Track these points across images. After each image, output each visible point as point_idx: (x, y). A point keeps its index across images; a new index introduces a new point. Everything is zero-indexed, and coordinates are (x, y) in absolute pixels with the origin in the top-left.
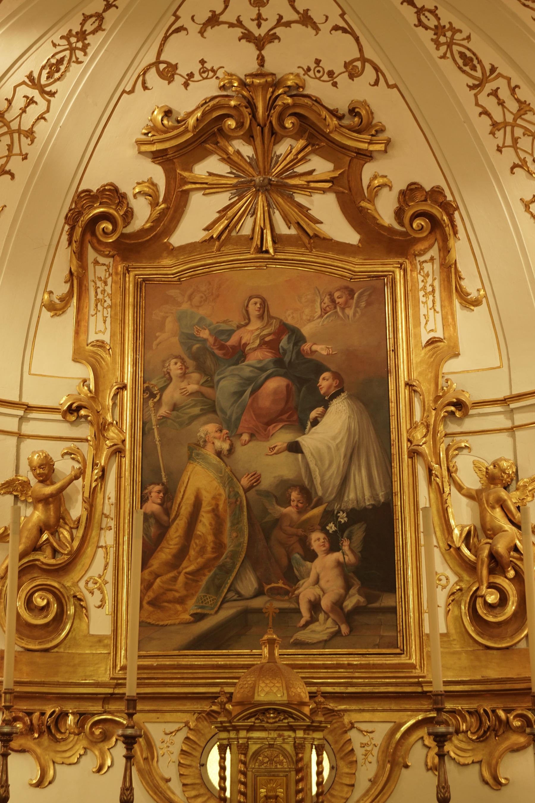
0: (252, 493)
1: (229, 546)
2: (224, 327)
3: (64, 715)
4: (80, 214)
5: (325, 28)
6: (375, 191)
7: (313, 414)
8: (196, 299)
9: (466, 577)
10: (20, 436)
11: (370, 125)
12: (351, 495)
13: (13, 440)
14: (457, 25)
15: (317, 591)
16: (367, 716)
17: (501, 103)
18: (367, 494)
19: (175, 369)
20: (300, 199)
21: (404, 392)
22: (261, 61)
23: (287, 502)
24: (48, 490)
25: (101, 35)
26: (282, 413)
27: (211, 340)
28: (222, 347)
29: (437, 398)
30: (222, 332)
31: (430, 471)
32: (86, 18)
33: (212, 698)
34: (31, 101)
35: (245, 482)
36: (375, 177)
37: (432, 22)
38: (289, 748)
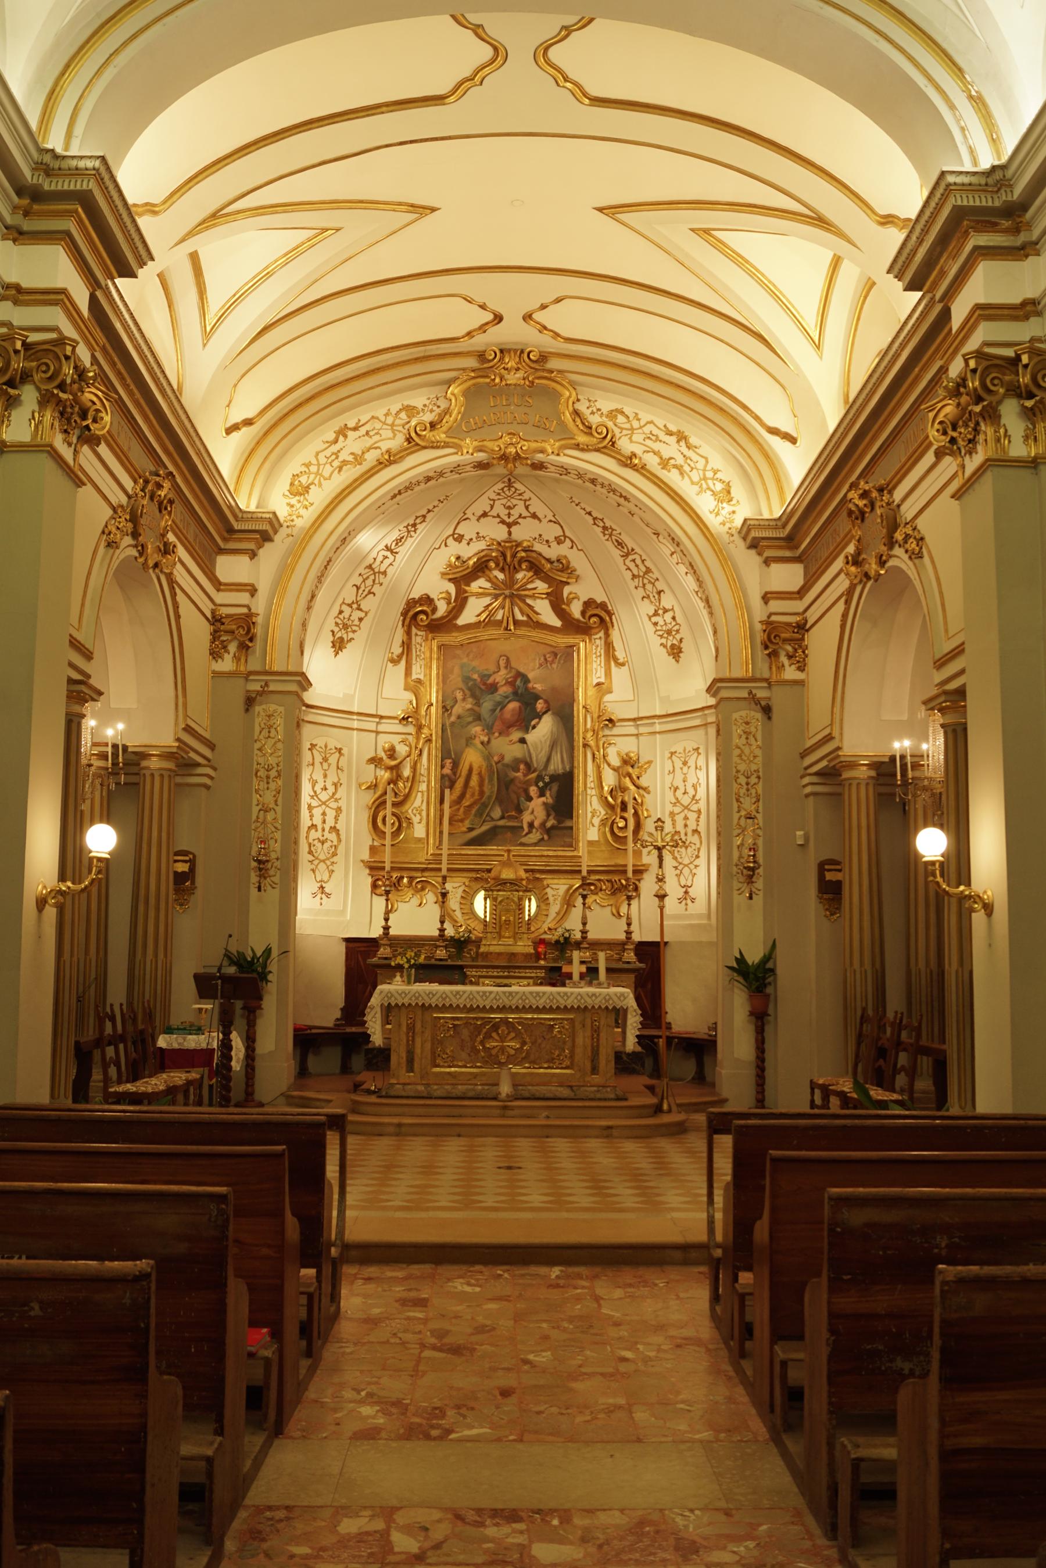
0: (499, 765)
1: (487, 793)
2: (486, 672)
3: (402, 878)
4: (409, 611)
5: (544, 521)
6: (569, 602)
7: (533, 723)
8: (471, 656)
9: (609, 812)
10: (377, 733)
11: (568, 568)
12: (552, 768)
13: (374, 735)
14: (614, 527)
15: (532, 817)
16: (556, 881)
17: (637, 566)
18: (560, 767)
19: (459, 695)
20: (529, 601)
21: (582, 711)
22: (510, 533)
23: (518, 770)
24: (393, 763)
25: (424, 524)
26: (517, 721)
27: (479, 680)
28: (485, 684)
29: (599, 716)
30: (485, 675)
31: (594, 755)
32: (417, 517)
33: (477, 871)
34: (386, 557)
35: (496, 759)
36: (571, 593)
37: (601, 524)
38: (516, 899)
